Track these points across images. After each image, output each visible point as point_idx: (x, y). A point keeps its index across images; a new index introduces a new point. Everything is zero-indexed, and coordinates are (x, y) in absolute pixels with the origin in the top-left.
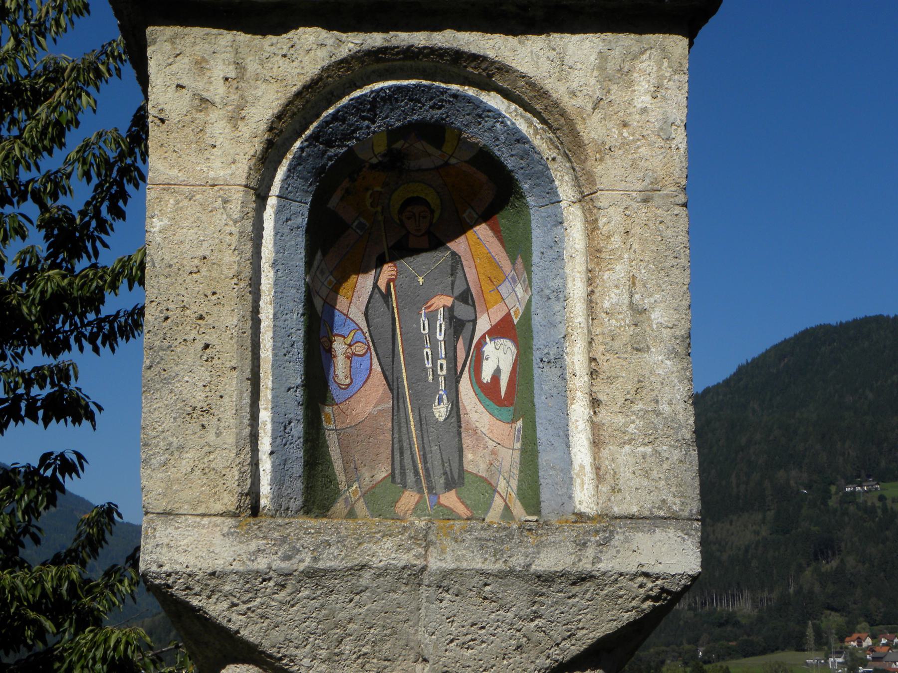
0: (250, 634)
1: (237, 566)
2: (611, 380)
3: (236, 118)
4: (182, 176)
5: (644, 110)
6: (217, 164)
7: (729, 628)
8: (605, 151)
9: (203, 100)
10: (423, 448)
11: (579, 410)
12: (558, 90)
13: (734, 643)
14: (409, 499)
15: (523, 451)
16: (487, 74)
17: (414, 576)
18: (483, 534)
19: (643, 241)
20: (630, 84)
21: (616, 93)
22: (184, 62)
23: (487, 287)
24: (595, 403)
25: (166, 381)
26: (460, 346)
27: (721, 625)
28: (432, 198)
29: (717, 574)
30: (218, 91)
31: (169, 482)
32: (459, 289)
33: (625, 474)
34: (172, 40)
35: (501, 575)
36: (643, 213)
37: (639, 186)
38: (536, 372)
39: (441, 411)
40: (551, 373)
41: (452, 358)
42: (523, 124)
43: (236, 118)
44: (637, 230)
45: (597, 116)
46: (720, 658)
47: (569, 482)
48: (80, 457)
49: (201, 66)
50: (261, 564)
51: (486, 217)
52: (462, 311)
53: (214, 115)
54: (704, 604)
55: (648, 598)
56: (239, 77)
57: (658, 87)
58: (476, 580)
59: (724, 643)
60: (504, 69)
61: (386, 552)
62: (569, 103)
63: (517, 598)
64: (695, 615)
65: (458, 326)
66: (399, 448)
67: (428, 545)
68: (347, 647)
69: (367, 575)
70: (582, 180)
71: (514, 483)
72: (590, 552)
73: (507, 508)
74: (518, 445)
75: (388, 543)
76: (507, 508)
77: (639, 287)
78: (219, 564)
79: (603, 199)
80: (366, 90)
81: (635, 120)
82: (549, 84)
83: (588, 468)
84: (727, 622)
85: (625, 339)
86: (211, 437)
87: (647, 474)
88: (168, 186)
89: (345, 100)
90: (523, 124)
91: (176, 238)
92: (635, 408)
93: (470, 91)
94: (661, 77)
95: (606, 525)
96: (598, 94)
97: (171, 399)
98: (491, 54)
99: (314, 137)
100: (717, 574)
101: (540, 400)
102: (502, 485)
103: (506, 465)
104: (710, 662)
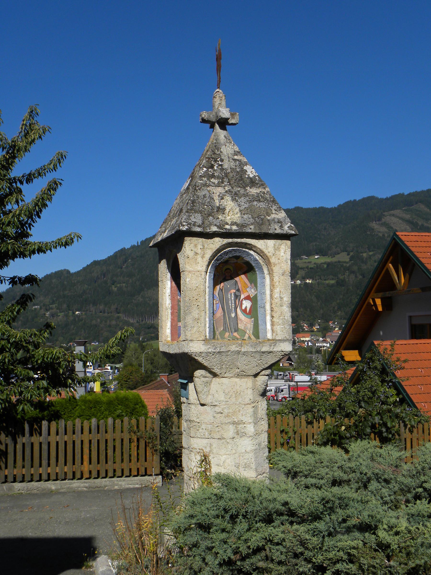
0: (206, 364)
1: (205, 351)
2: (276, 312)
3: (203, 257)
4: (192, 269)
5: (282, 256)
6: (199, 267)
7: (152, 329)
8: (275, 265)
9: (196, 253)
10: (229, 323)
11: (268, 318)
12: (266, 252)
13: (153, 335)
14: (227, 334)
15: (254, 325)
16: (251, 247)
17: (239, 352)
18: (252, 344)
19: (282, 283)
20: (280, 251)
21: (277, 252)
22: (192, 245)
23: (243, 289)
24: (272, 317)
25: (190, 313)
26: (237, 301)
27: (149, 328)
28: (231, 268)
29: (148, 309)
30: (199, 251)
31: (192, 334)
32: (237, 289)
33: (279, 331)
34: (190, 240)
35: (255, 352)
36: (282, 277)
37: (282, 272)
38: (259, 309)
39: (233, 315)
40: (262, 310)
41: (235, 303)
42: (257, 257)
43: (203, 257)
44: (281, 281)
45: (274, 257)
46: (148, 340)
47: (266, 333)
48: (33, 295)
49: (196, 246)
50: (210, 350)
51: (244, 273)
52: (237, 293)
53: (198, 256)
54: (142, 321)
55: (282, 355)
56: (203, 248)
57: (285, 251)
58: (251, 353)
59: (150, 335)
60: (255, 247)
61: (234, 348)
62: (268, 255)
63: (258, 356)
64: (139, 325)
65: (237, 297)
66: (225, 323)
67: (242, 346)
68: (224, 366)
69: (230, 352)
70: (270, 270)
71: (251, 332)
72: (272, 347)
73: (249, 336)
74: (252, 324)
75: (234, 346)
76: (249, 336)
77: (281, 293)
78: (202, 351)
79: (275, 274)
80: (227, 250)
81: (281, 258)
82: (264, 250)
83: (270, 330)
84: (151, 327)
85: (279, 304)
86: (199, 325)
87: (282, 331)
88: (190, 272)
89: (222, 252)
90: (257, 257)
91: (191, 283)
92: (281, 318)
93: (247, 250)
94: (286, 249)
95: (275, 341)
96: (274, 253)
97: (191, 317)
98: (253, 244)
99: (216, 260)
100: (148, 309)
101: (259, 315)
102: (248, 332)
103: (249, 327)
104: (144, 342)
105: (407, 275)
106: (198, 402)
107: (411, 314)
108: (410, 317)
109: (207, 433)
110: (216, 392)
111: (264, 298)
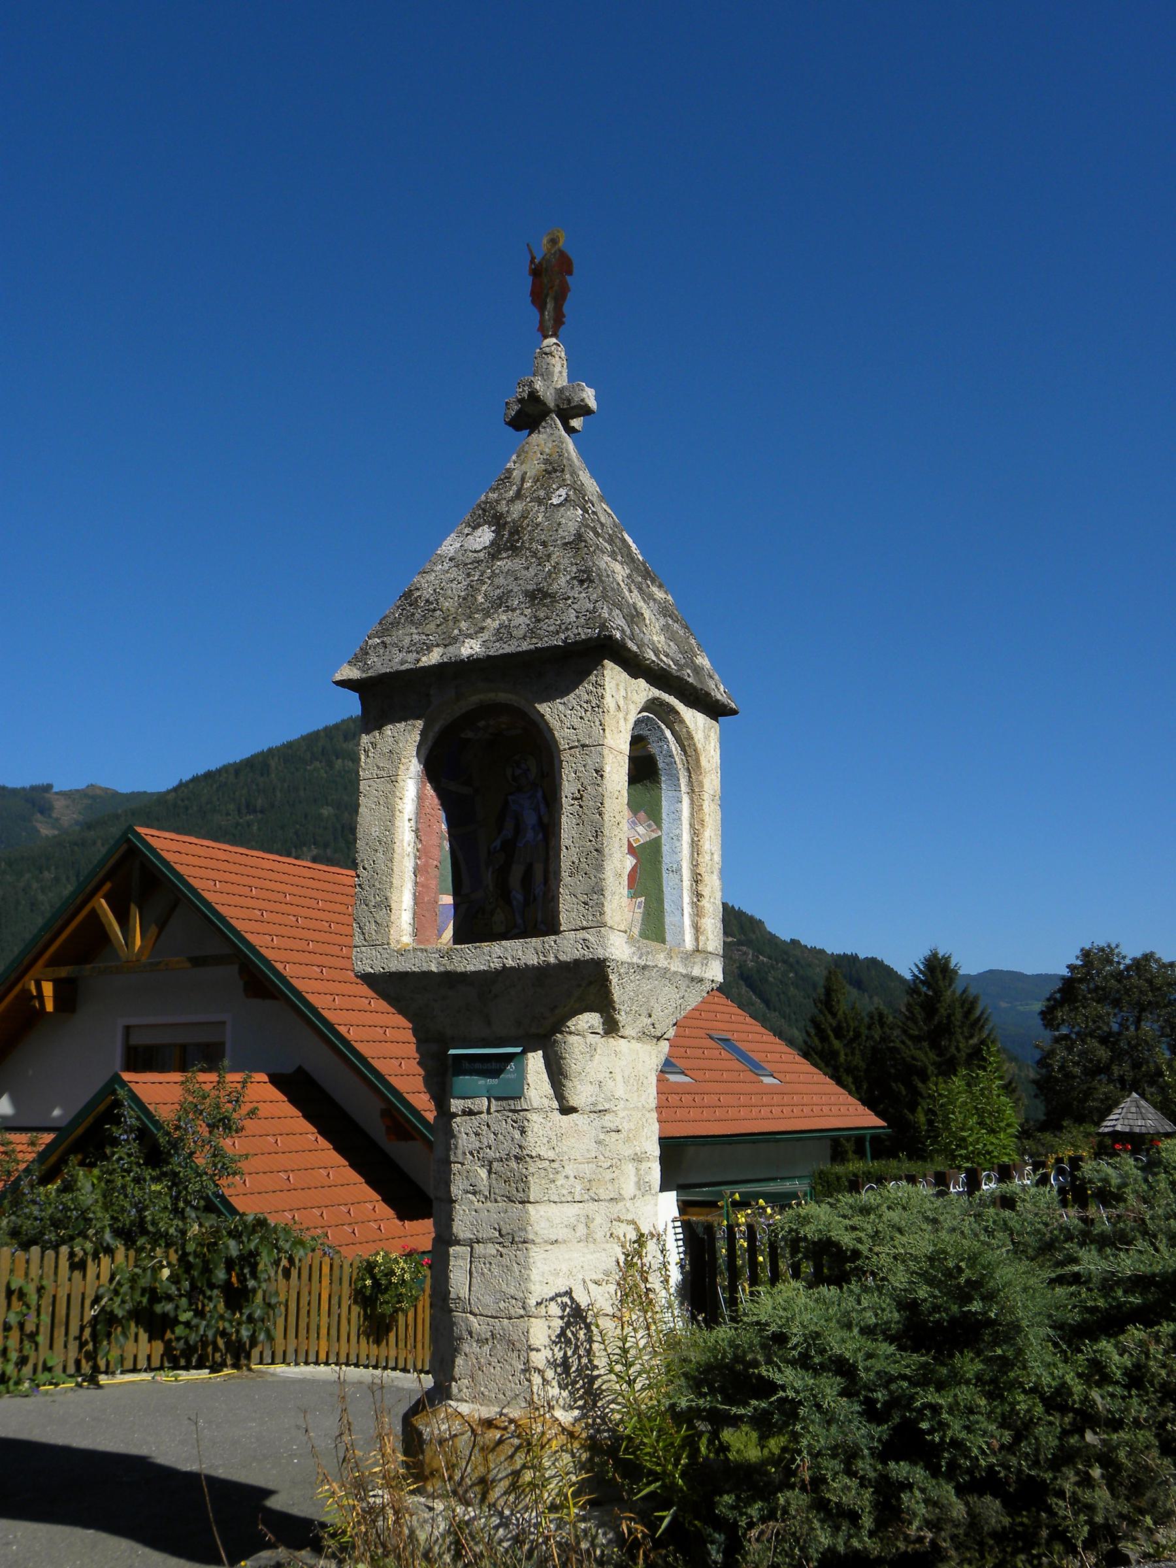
38: (665, 875)
93: (663, 727)
105: (153, 930)
106: (556, 1105)
107: (133, 1021)
108: (127, 1029)
109: (578, 1188)
110: (608, 1075)
111: (678, 850)
